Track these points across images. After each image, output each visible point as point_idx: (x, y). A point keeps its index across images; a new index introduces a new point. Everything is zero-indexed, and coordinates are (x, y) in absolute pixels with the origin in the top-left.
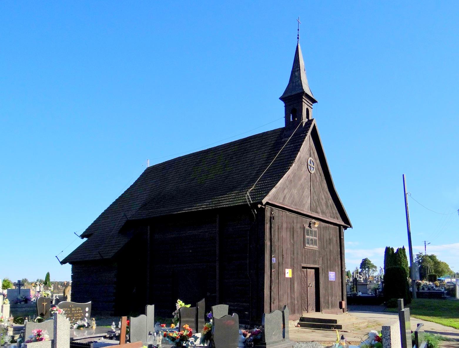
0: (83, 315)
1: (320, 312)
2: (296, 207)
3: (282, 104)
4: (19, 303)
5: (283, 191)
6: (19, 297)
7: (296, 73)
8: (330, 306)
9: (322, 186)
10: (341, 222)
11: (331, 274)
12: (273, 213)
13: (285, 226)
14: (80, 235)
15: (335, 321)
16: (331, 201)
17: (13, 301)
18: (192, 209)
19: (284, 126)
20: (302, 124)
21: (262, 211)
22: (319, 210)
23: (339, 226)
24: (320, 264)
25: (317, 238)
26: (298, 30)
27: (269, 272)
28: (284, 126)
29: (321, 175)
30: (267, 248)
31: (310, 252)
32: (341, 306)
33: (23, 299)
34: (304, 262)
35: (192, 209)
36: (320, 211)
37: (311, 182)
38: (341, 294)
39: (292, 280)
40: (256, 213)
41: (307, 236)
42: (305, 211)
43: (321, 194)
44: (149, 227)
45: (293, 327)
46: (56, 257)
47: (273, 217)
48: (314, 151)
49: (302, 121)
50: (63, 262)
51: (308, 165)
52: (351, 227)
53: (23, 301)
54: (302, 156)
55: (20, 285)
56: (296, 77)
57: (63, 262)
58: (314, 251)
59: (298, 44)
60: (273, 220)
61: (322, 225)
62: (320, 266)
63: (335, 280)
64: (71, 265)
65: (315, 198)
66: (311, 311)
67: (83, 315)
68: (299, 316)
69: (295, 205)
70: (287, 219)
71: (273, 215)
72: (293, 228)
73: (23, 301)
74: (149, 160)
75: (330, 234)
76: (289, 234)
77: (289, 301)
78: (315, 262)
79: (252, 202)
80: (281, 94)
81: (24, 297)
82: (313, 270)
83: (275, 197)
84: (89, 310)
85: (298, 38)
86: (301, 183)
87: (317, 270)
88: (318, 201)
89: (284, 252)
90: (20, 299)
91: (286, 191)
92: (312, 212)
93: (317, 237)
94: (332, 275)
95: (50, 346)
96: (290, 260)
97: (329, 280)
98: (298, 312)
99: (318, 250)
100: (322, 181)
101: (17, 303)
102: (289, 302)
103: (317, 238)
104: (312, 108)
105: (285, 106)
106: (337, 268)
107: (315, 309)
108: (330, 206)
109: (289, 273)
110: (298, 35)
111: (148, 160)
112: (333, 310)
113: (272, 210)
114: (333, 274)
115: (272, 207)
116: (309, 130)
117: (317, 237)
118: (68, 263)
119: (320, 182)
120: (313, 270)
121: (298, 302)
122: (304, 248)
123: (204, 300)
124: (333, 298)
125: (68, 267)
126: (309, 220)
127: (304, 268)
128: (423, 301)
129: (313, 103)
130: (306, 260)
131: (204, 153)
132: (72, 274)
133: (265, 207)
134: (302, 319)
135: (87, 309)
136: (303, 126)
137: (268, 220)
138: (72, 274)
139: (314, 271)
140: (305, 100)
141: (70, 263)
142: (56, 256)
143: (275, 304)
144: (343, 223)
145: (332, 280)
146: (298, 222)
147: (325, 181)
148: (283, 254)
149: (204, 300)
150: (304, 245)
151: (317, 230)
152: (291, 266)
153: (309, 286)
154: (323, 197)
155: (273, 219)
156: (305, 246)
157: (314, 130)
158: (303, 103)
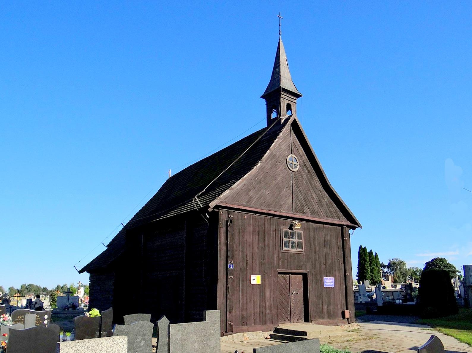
0: (41, 322)
1: (309, 322)
2: (267, 209)
3: (264, 102)
4: (67, 310)
5: (247, 194)
6: (68, 304)
7: (277, 70)
8: (326, 316)
9: (311, 184)
10: (345, 222)
11: (327, 280)
12: (229, 216)
13: (250, 229)
14: (107, 245)
15: (305, 334)
16: (327, 198)
17: (62, 307)
18: (164, 217)
20: (281, 119)
21: (215, 215)
22: (306, 209)
23: (342, 226)
24: (308, 268)
25: (302, 241)
27: (224, 280)
29: (309, 172)
30: (222, 253)
31: (291, 256)
32: (343, 316)
33: (71, 305)
35: (164, 217)
36: (308, 210)
37: (293, 181)
38: (344, 302)
39: (261, 288)
40: (208, 217)
41: (285, 239)
42: (283, 212)
43: (309, 192)
45: (263, 339)
47: (231, 221)
48: (298, 147)
49: (279, 117)
50: (81, 272)
51: (288, 163)
52: (359, 227)
53: (71, 307)
54: (278, 153)
55: (69, 292)
56: (276, 73)
57: (81, 272)
58: (299, 255)
59: (279, 41)
60: (231, 224)
61: (313, 226)
62: (308, 271)
63: (334, 287)
64: (89, 274)
65: (300, 198)
66: (297, 321)
67: (41, 322)
68: (274, 326)
70: (253, 221)
71: (230, 219)
72: (264, 231)
73: (71, 307)
74: (170, 171)
75: (325, 235)
76: (257, 239)
77: (257, 310)
78: (299, 267)
79: (202, 207)
80: (262, 93)
81: (71, 304)
82: (301, 276)
83: (234, 198)
85: (280, 34)
86: (277, 182)
87: (305, 276)
88: (305, 201)
89: (248, 257)
90: (68, 305)
91: (251, 193)
92: (295, 213)
93: (303, 239)
94: (329, 282)
95: (167, 352)
96: (258, 265)
97: (324, 287)
98: (272, 322)
99: (304, 253)
100: (312, 178)
101: (65, 309)
102: (256, 311)
103: (303, 241)
104: (296, 103)
105: (267, 104)
106: (337, 273)
107: (303, 319)
108: (326, 205)
109: (256, 280)
110: (280, 31)
111: (169, 170)
112: (330, 320)
113: (229, 213)
114: (332, 280)
115: (228, 210)
116: (285, 126)
117: (303, 239)
118: (86, 272)
119: (309, 180)
120: (301, 276)
121: (271, 311)
122: (281, 252)
123: (111, 309)
124: (331, 307)
126: (289, 221)
127: (280, 273)
129: (297, 98)
130: (286, 265)
132: (90, 283)
133: (219, 211)
134: (277, 330)
135: (46, 317)
137: (224, 224)
138: (90, 283)
139: (302, 277)
140: (283, 95)
141: (88, 272)
143: (234, 313)
145: (329, 286)
146: (270, 225)
147: (317, 178)
148: (247, 259)
149: (111, 309)
150: (282, 249)
151: (302, 231)
152: (260, 272)
153: (293, 293)
154: (314, 195)
155: (231, 222)
156: (283, 250)
157: (295, 126)
158: (282, 99)
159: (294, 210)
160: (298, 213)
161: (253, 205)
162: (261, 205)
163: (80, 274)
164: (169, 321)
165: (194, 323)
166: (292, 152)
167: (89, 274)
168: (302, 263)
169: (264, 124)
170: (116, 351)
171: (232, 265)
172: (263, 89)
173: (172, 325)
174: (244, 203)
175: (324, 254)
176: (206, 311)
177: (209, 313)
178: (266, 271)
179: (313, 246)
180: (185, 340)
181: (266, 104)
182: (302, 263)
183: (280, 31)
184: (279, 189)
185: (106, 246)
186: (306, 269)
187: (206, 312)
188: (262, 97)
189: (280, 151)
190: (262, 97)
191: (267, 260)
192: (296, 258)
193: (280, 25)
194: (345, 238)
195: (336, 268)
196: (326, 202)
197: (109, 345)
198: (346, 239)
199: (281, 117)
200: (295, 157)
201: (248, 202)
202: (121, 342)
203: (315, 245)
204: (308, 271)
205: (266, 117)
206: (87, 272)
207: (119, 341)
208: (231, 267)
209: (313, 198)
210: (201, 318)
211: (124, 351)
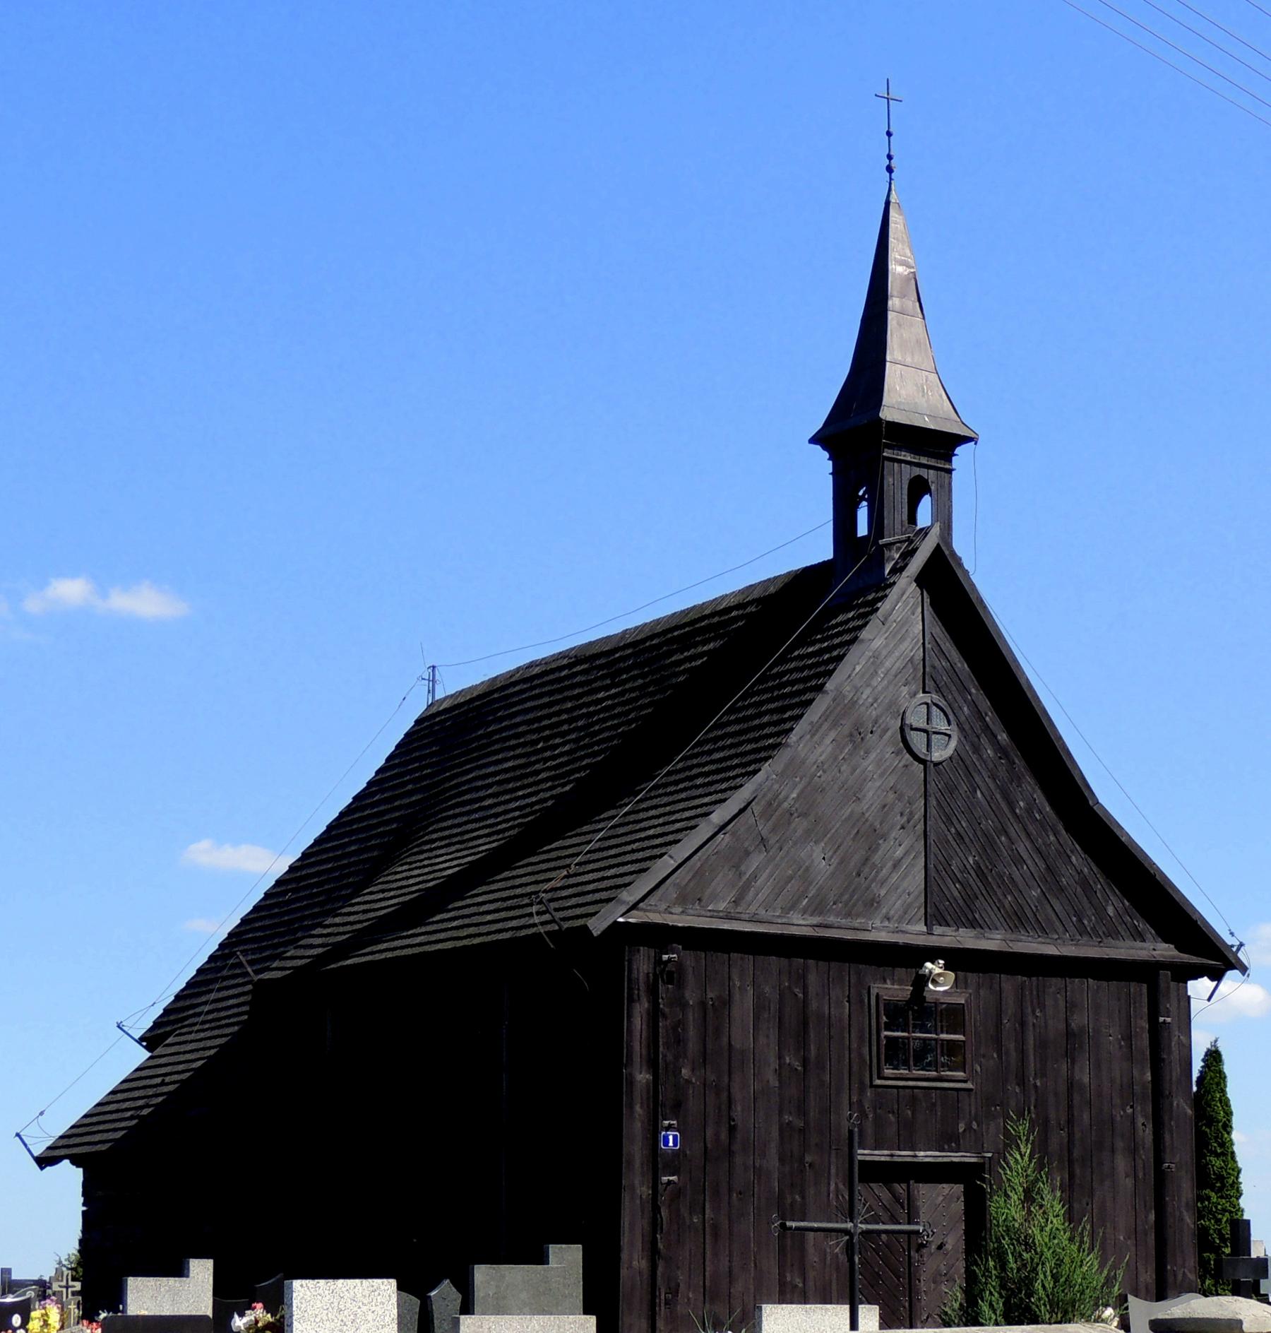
3: (822, 462)
5: (736, 867)
19: (829, 555)
23: (1145, 972)
26: (889, 134)
28: (829, 555)
34: (870, 1140)
44: (574, 970)
46: (17, 1138)
50: (44, 1161)
64: (81, 1170)
69: (818, 907)
84: (11, 1320)
85: (890, 169)
106: (1121, 1163)
107: (581, 1305)
110: (890, 157)
125: (70, 1177)
128: (685, 1263)
131: (948, 520)
132: (85, 1208)
136: (432, 739)
138: (85, 1208)
141: (76, 1161)
142: (18, 1135)
144: (1164, 951)
148: (734, 1114)
154: (1023, 847)
159: (934, 917)
160: (949, 926)
161: (762, 912)
162: (792, 907)
163: (42, 1168)
164: (460, 1296)
165: (522, 1266)
166: (929, 682)
167: (81, 1170)
168: (962, 1127)
169: (821, 549)
170: (379, 1304)
171: (675, 1137)
172: (818, 415)
173: (479, 1267)
174: (722, 906)
175: (1062, 1088)
176: (550, 1246)
177: (557, 1250)
178: (808, 1159)
179: (1013, 1054)
180: (504, 1298)
181: (831, 471)
182: (962, 1127)
183: (890, 157)
184: (872, 837)
185: (137, 1038)
186: (979, 1151)
187: (550, 1249)
188: (813, 441)
189: (874, 683)
190: (813, 441)
191: (813, 1114)
192: (934, 1105)
193: (889, 134)
194: (1161, 1019)
195: (1120, 1144)
196: (1080, 873)
197: (366, 1293)
198: (1169, 1020)
199: (881, 542)
200: (943, 703)
201: (736, 903)
202: (386, 1288)
203: (1022, 1053)
204: (990, 1155)
205: (832, 518)
206: (73, 1163)
207: (382, 1287)
208: (671, 1144)
209: (1018, 860)
210: (540, 1258)
211: (391, 1306)
